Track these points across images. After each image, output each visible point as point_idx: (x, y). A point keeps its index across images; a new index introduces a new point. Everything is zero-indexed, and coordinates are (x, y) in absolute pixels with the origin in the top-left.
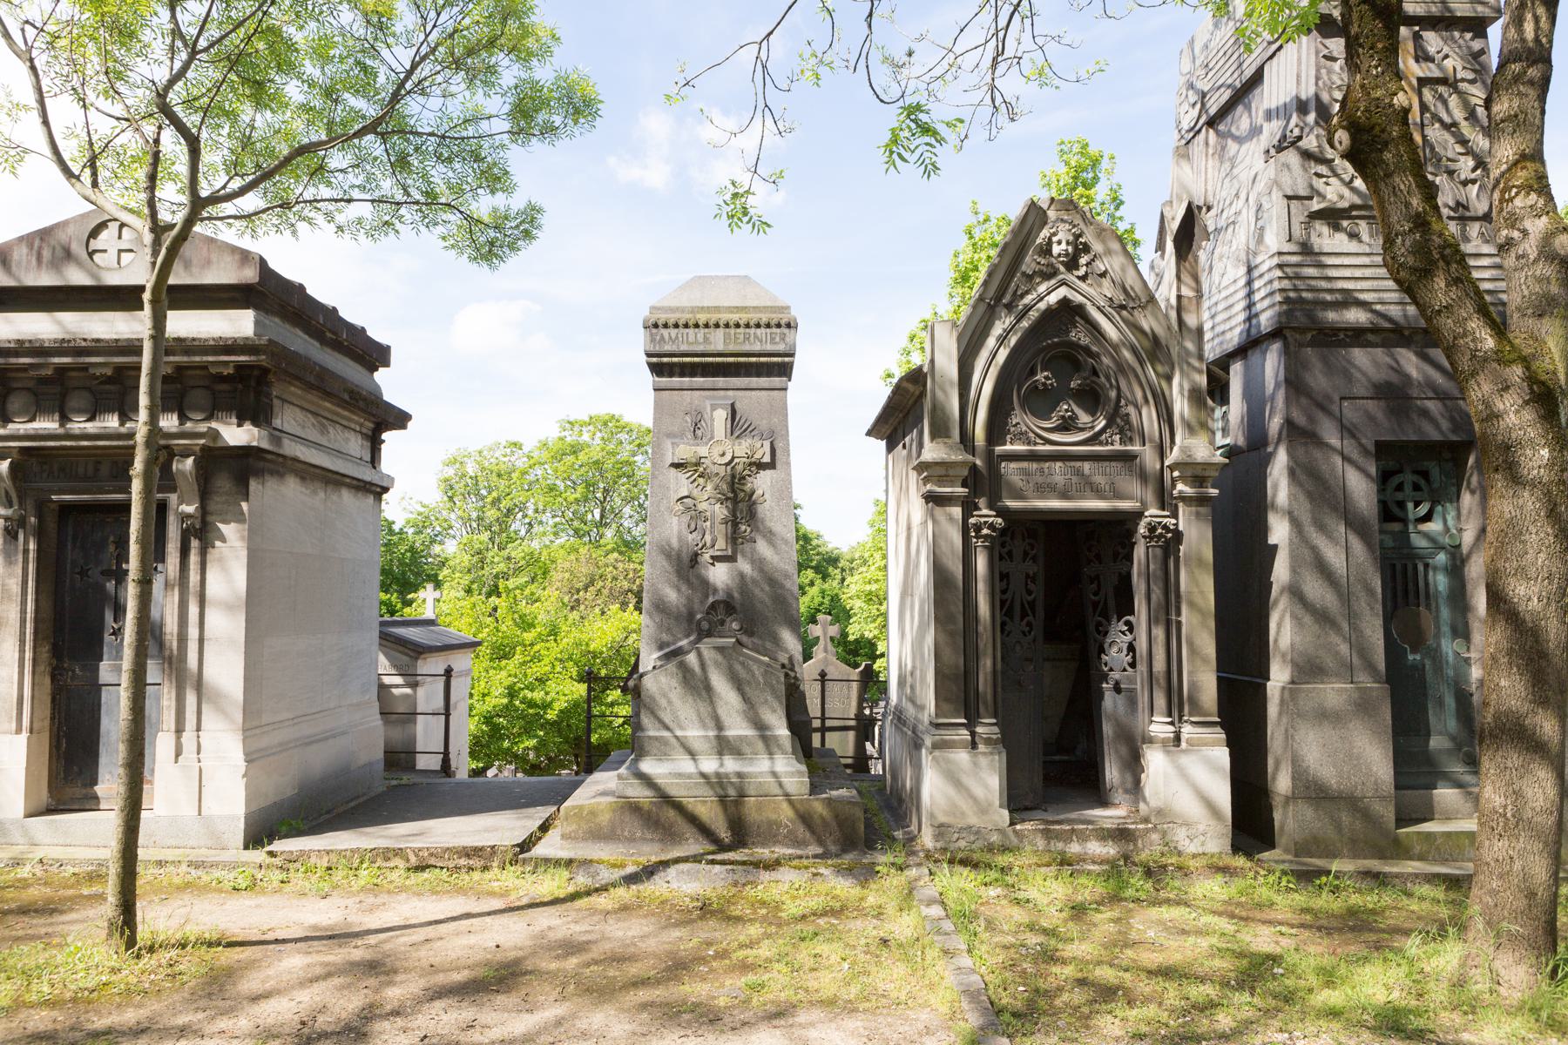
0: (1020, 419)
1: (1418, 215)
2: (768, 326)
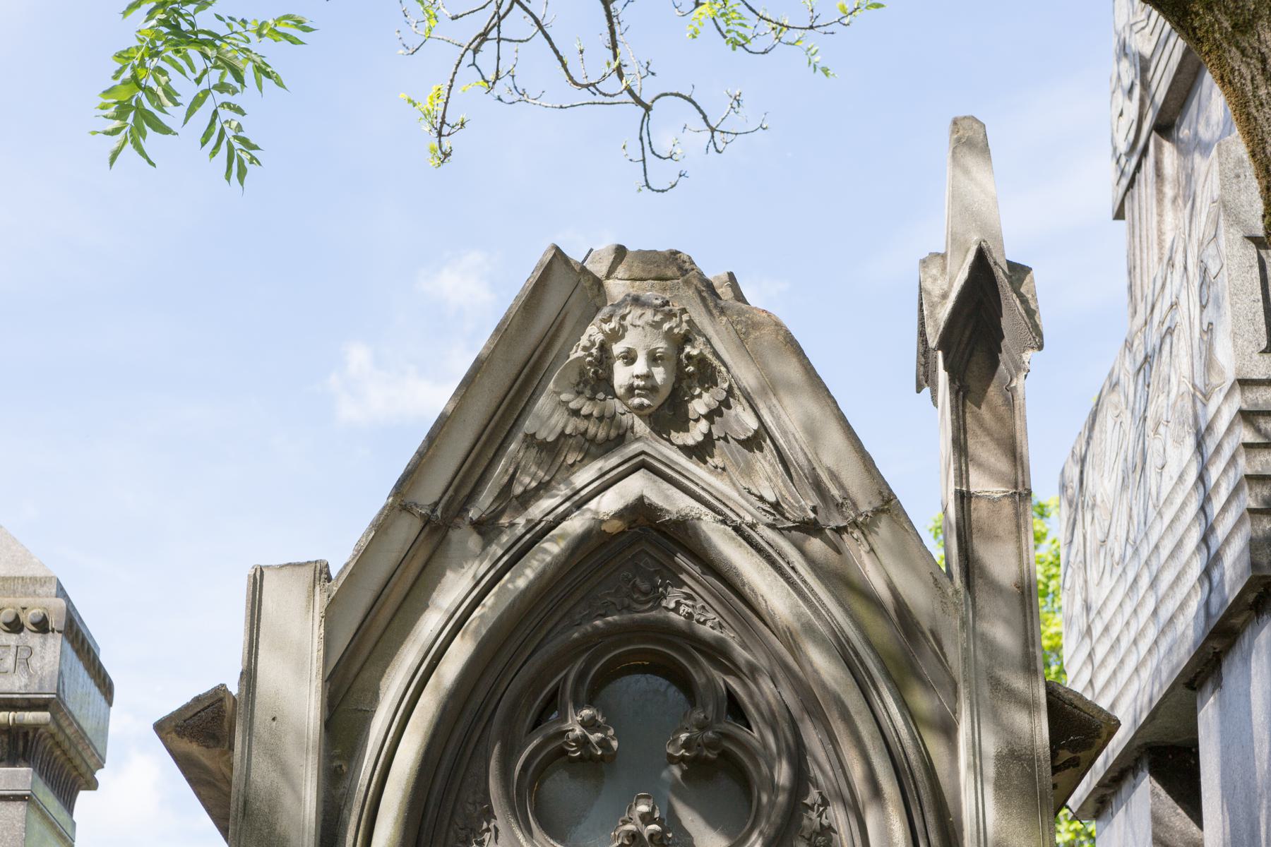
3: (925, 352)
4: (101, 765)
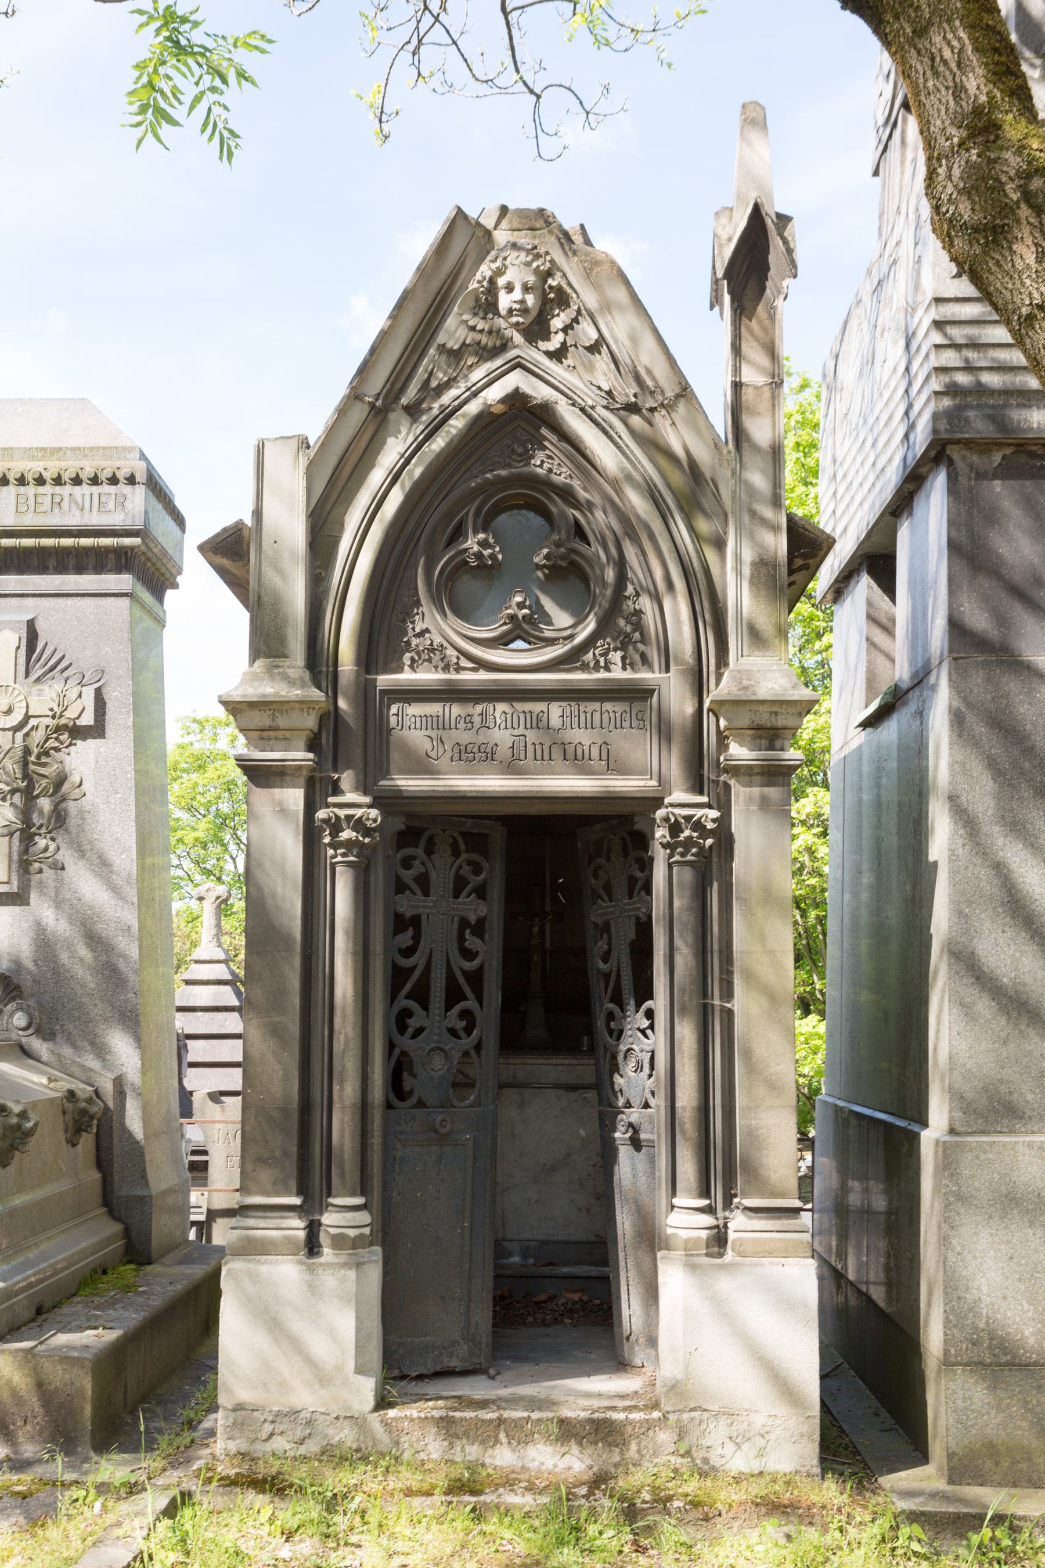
0: (434, 625)
1: (977, 111)
2: (95, 481)
3: (716, 282)
4: (180, 573)
